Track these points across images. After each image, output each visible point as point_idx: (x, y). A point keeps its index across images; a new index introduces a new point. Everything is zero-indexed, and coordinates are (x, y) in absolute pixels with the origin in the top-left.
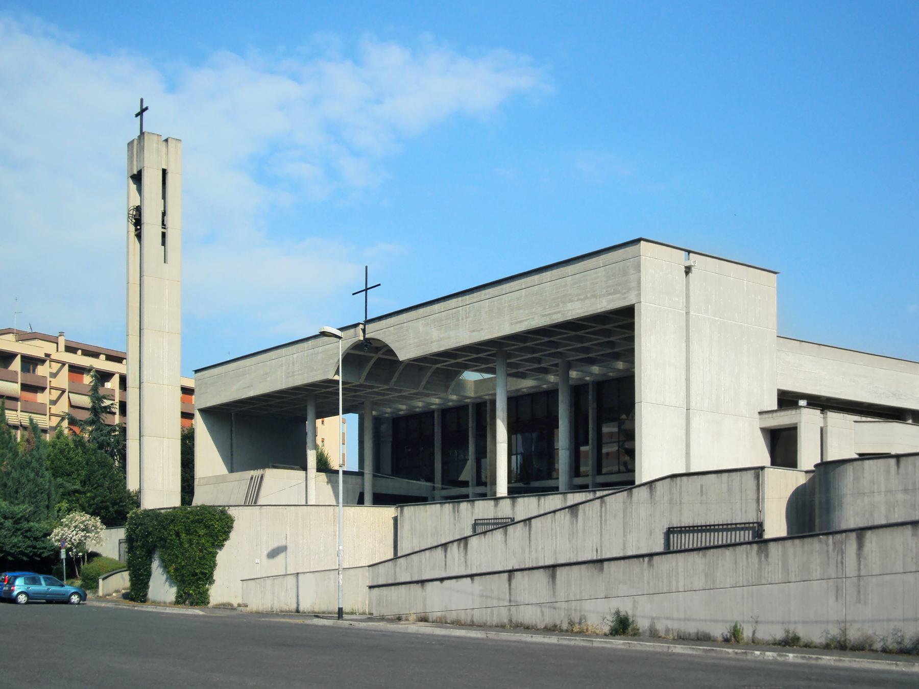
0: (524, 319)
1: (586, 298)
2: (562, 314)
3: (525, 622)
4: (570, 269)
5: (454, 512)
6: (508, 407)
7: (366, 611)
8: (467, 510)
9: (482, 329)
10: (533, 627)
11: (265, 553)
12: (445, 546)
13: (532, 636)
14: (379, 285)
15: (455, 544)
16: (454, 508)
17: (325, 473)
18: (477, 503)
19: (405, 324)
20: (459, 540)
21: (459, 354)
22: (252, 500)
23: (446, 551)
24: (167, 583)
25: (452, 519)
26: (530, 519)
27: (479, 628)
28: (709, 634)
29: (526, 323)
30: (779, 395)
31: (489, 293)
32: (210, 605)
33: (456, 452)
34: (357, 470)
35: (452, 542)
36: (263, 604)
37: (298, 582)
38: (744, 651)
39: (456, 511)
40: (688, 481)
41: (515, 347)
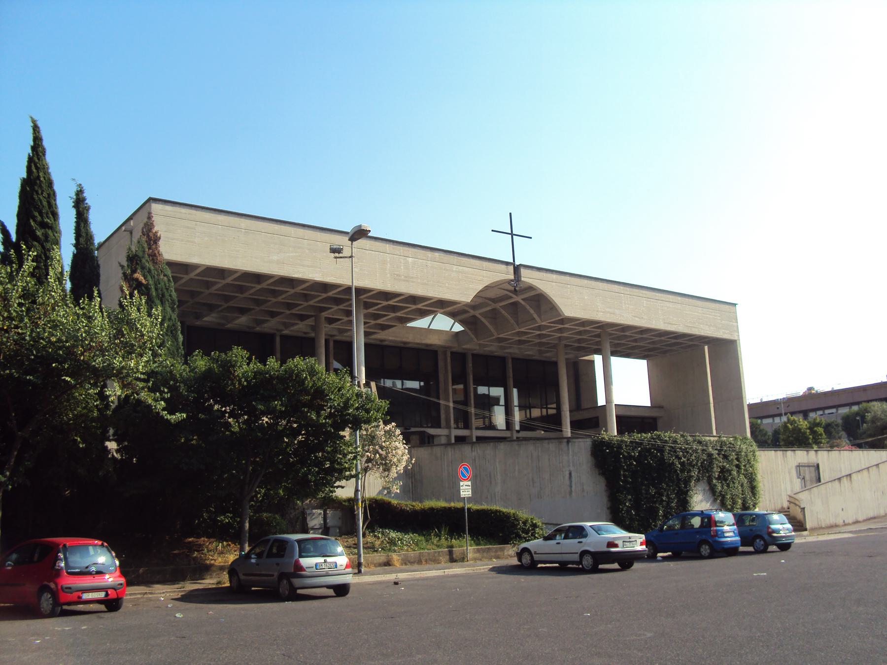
5: (783, 457)
7: (94, 550)
8: (791, 456)
10: (815, 528)
12: (839, 479)
15: (845, 478)
16: (783, 454)
17: (464, 389)
18: (796, 452)
20: (847, 476)
21: (310, 294)
23: (840, 482)
25: (783, 462)
26: (878, 464)
29: (676, 326)
33: (312, 390)
34: (650, 406)
35: (843, 477)
39: (784, 456)
40: (863, 453)
41: (549, 330)
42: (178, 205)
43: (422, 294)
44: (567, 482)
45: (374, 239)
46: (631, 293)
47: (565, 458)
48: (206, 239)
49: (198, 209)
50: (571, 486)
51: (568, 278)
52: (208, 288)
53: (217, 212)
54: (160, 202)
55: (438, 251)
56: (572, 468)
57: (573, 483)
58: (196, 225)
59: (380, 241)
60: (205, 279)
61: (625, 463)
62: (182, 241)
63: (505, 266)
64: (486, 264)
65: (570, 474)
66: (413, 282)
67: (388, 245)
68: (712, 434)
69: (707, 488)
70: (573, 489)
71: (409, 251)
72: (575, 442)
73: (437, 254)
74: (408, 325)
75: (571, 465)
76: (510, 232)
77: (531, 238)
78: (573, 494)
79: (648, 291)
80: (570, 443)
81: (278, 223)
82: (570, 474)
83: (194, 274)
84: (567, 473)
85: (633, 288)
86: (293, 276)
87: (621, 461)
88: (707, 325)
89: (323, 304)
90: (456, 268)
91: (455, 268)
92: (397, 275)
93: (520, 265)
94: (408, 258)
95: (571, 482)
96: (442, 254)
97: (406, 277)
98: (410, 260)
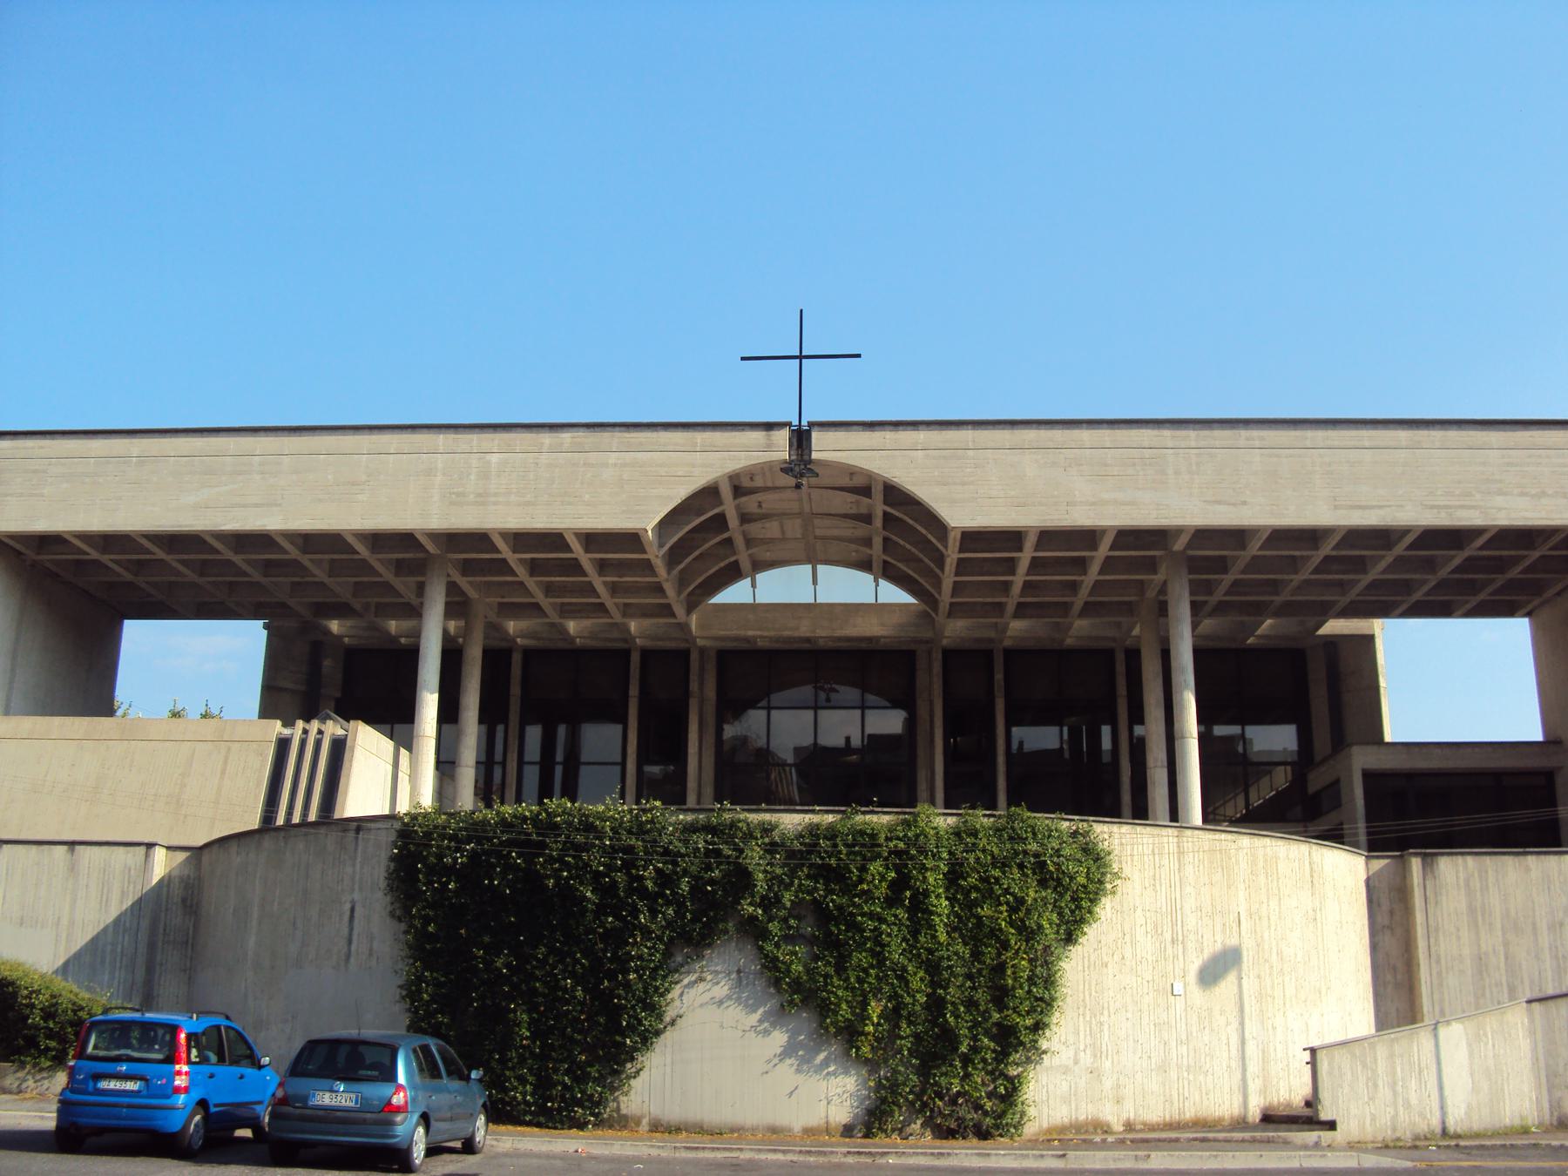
0: (1374, 504)
1: (1544, 494)
2: (1481, 512)
3: (1464, 1128)
4: (1494, 437)
6: (416, 677)
9: (1244, 503)
11: (1195, 964)
13: (1233, 1156)
14: (858, 356)
19: (970, 453)
22: (1498, 816)
24: (782, 1048)
27: (1263, 1145)
28: (660, 1120)
29: (1382, 512)
30: (263, 718)
31: (1262, 439)
32: (1030, 1129)
36: (1373, 1119)
37: (1437, 1045)
38: (1061, 1153)
42: (8, 437)
43: (475, 527)
44: (345, 931)
45: (491, 430)
46: (1202, 444)
47: (349, 870)
48: (65, 485)
49: (56, 436)
50: (350, 942)
51: (967, 435)
52: (1210, 593)
53: (91, 436)
54: (901, 428)
55: (571, 429)
56: (356, 896)
57: (355, 933)
58: (49, 465)
59: (425, 430)
60: (1466, 576)
61: (429, 883)
62: (20, 496)
63: (764, 433)
64: (700, 437)
65: (352, 910)
66: (495, 503)
67: (441, 436)
68: (1188, 823)
69: (755, 967)
70: (353, 948)
71: (493, 440)
72: (370, 829)
73: (566, 436)
74: (710, 602)
75: (356, 887)
76: (803, 354)
77: (743, 359)
78: (352, 960)
79: (1357, 429)
80: (361, 833)
81: (1151, 425)
82: (352, 910)
83: (1449, 570)
84: (348, 906)
85: (1212, 429)
86: (223, 528)
87: (419, 881)
88: (1522, 494)
89: (573, 582)
90: (613, 453)
91: (613, 458)
92: (458, 494)
93: (811, 424)
94: (488, 456)
95: (351, 929)
96: (581, 435)
97: (480, 495)
98: (494, 458)
